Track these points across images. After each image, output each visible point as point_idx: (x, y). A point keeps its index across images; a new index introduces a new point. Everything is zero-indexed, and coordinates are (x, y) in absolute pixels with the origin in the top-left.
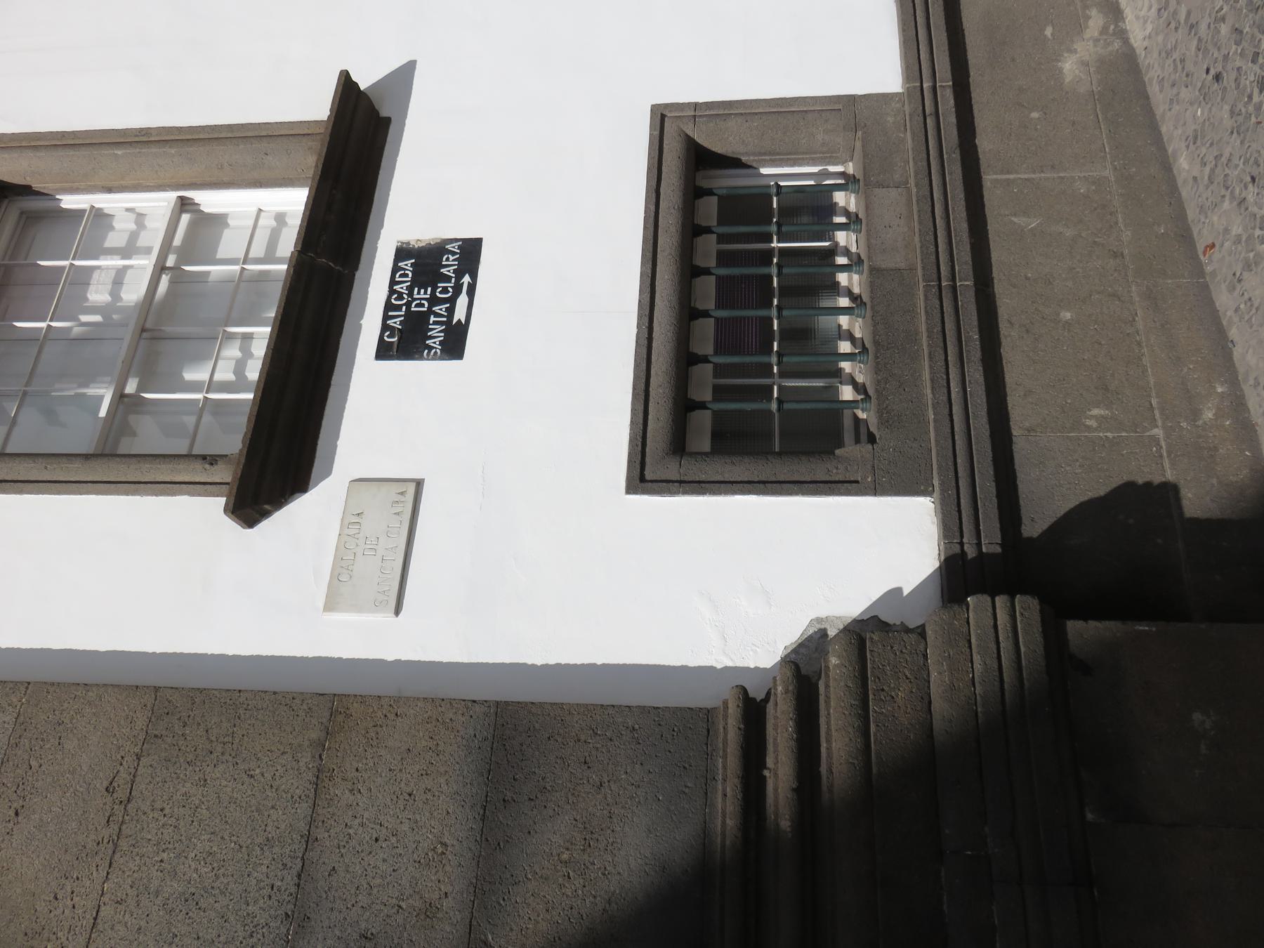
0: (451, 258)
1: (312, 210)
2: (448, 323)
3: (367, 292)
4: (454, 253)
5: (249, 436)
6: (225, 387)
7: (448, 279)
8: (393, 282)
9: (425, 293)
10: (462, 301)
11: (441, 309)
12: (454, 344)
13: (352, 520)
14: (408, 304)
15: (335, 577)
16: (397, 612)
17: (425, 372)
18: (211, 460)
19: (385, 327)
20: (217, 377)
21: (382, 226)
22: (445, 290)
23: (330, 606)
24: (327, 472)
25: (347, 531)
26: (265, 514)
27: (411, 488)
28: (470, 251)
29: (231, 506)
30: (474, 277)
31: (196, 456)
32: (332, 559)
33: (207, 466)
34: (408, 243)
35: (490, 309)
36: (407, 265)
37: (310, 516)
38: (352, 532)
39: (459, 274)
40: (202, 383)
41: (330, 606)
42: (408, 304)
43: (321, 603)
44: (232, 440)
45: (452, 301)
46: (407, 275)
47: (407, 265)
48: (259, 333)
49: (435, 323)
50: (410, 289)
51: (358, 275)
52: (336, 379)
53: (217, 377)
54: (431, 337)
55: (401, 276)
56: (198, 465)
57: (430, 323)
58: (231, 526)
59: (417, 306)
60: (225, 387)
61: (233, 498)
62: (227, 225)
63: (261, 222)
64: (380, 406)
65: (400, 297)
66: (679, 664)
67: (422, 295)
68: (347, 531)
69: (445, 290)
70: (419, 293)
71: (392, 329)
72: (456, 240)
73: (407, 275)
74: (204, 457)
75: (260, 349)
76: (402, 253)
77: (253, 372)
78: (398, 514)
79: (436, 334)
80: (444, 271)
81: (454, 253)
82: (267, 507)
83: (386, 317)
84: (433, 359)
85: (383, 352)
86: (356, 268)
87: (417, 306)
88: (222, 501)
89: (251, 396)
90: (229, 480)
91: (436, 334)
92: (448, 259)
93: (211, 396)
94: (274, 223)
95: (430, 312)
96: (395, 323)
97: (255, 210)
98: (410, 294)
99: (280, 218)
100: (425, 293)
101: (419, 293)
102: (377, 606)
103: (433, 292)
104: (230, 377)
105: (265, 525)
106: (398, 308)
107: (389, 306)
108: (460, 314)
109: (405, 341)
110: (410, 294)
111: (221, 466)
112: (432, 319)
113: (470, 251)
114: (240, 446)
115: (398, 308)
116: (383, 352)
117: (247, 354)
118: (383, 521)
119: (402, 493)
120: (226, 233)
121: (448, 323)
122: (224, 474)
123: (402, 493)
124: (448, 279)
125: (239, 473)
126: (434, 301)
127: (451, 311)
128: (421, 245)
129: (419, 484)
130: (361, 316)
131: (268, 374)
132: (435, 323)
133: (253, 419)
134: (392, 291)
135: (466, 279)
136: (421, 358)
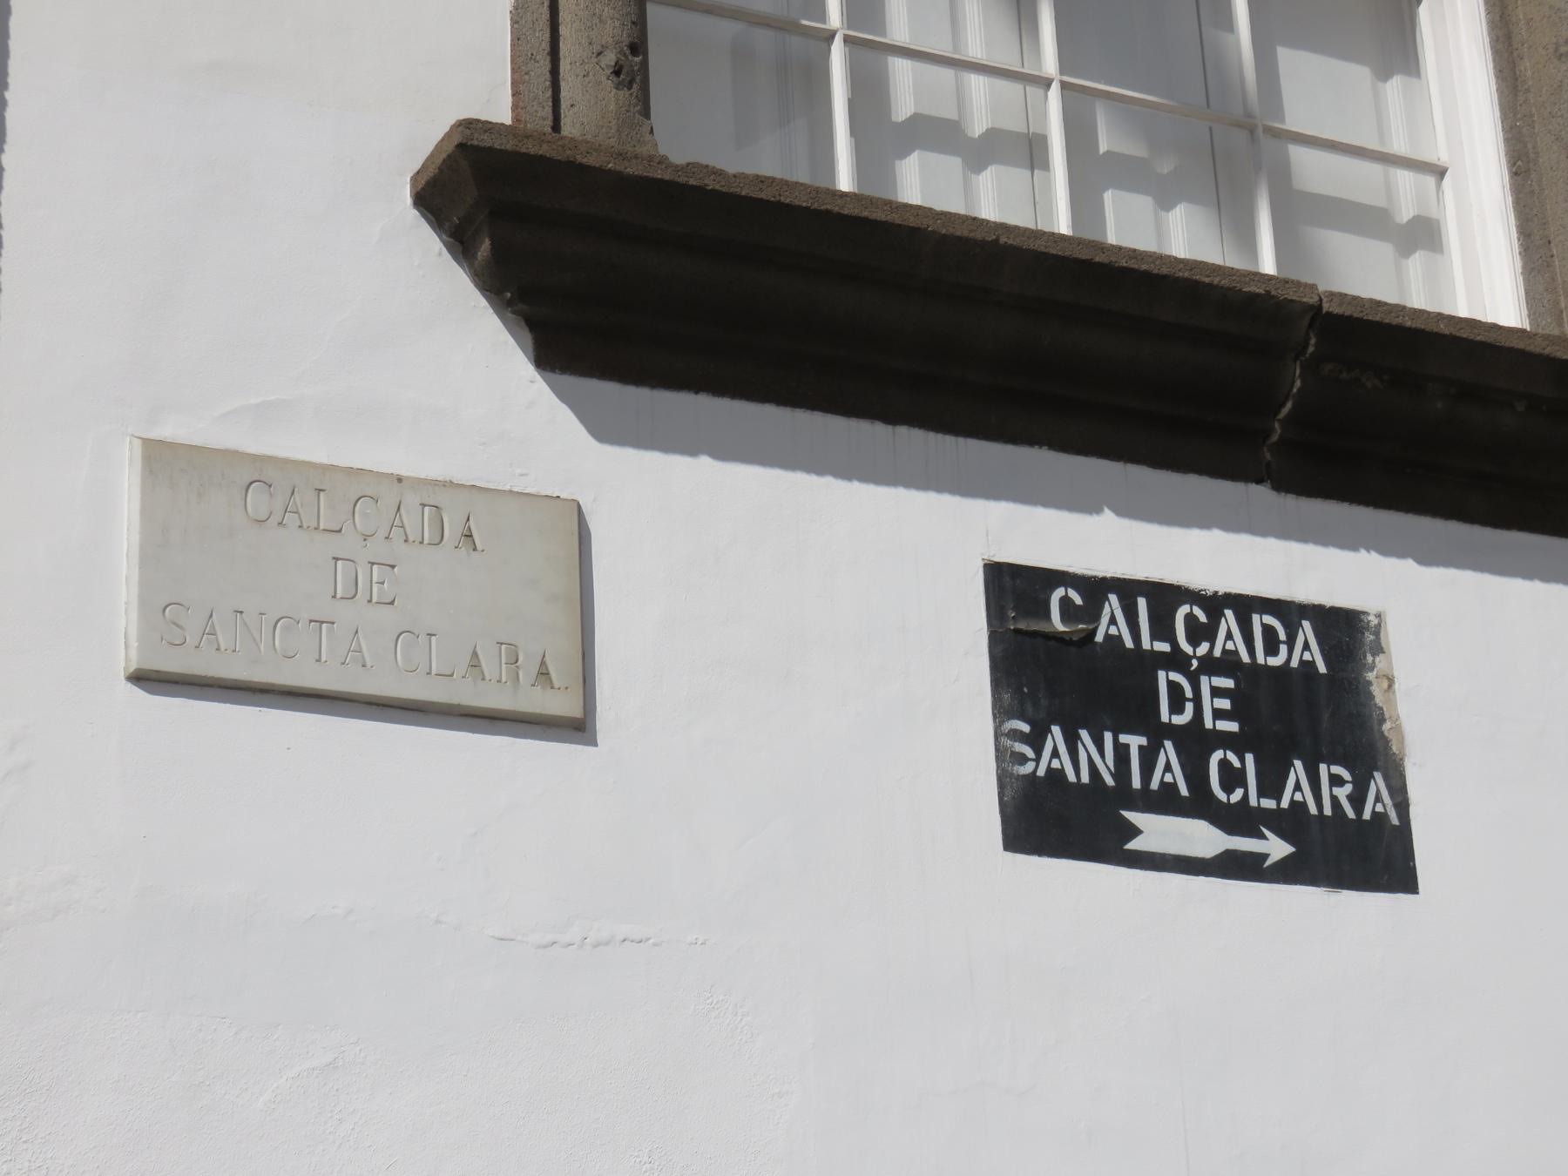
0: (1342, 793)
1: (1454, 340)
2: (1124, 796)
3: (1205, 524)
4: (1358, 800)
5: (711, 184)
6: (870, 93)
7: (1272, 784)
8: (1245, 606)
9: (1218, 714)
10: (1203, 838)
11: (1170, 767)
12: (1053, 820)
13: (451, 516)
14: (1176, 660)
15: (260, 472)
16: (143, 679)
17: (957, 732)
18: (631, 68)
19: (1095, 588)
20: (901, 68)
21: (1425, 560)
22: (1232, 778)
23: (163, 460)
24: (604, 430)
25: (412, 500)
26: (460, 242)
27: (563, 704)
28: (1367, 855)
29: (486, 141)
30: (1286, 873)
31: (640, 23)
32: (320, 456)
33: (610, 58)
34: (1378, 649)
35: (1187, 937)
36: (1307, 649)
37: (466, 388)
38: (410, 519)
39: (1291, 823)
40: (879, 23)
41: (163, 460)
42: (1176, 660)
43: (170, 430)
44: (703, 130)
45: (1200, 805)
46: (1271, 649)
47: (1307, 649)
48: (1048, 186)
49: (1122, 753)
50: (1225, 664)
51: (1261, 495)
52: (913, 440)
53: (901, 68)
54: (1072, 742)
55: (1269, 631)
56: (612, 31)
57: (1099, 730)
58: (420, 138)
59: (1174, 688)
60: (870, 93)
61: (509, 145)
62: (1384, 74)
63: (1404, 178)
64: (828, 596)
65: (1198, 633)
66: (903, 431)
67: (1212, 703)
68: (412, 500)
69: (1232, 778)
70: (1216, 692)
71: (1091, 612)
72: (1403, 806)
73: (1271, 649)
74: (638, 47)
75: (992, 199)
76: (1344, 631)
77: (922, 184)
78: (475, 663)
79: (1086, 758)
80: (1301, 764)
81: (1358, 800)
82: (484, 248)
83: (1128, 590)
84: (1000, 753)
85: (1014, 589)
86: (1281, 486)
87: (1174, 688)
88: (502, 114)
89: (845, 181)
90: (568, 129)
91: (1086, 758)
92: (1336, 781)
93: (837, 52)
94: (1405, 213)
95: (1158, 733)
96: (1111, 622)
97: (1441, 155)
98: (1211, 665)
99: (1423, 235)
100: (1218, 714)
101: (1216, 692)
102: (161, 609)
103: (1225, 740)
104: (904, 105)
105: (428, 243)
106: (1162, 628)
107: (1165, 597)
108: (1158, 831)
109: (1058, 658)
110: (1211, 665)
111: (613, 98)
112: (1135, 742)
113: (1367, 855)
114: (679, 157)
115: (1162, 628)
116: (1014, 589)
117: (983, 151)
118: (449, 617)
119: (543, 674)
120: (1359, 74)
121: (1124, 796)
122: (588, 113)
123: (543, 674)
124: (1272, 784)
125: (590, 160)
126: (1195, 743)
127: (1165, 802)
128: (1377, 691)
129: (579, 728)
130: (1126, 510)
131: (914, 231)
132: (1122, 753)
133: (766, 194)
134: (1215, 604)
135: (1276, 848)
136: (1001, 712)
